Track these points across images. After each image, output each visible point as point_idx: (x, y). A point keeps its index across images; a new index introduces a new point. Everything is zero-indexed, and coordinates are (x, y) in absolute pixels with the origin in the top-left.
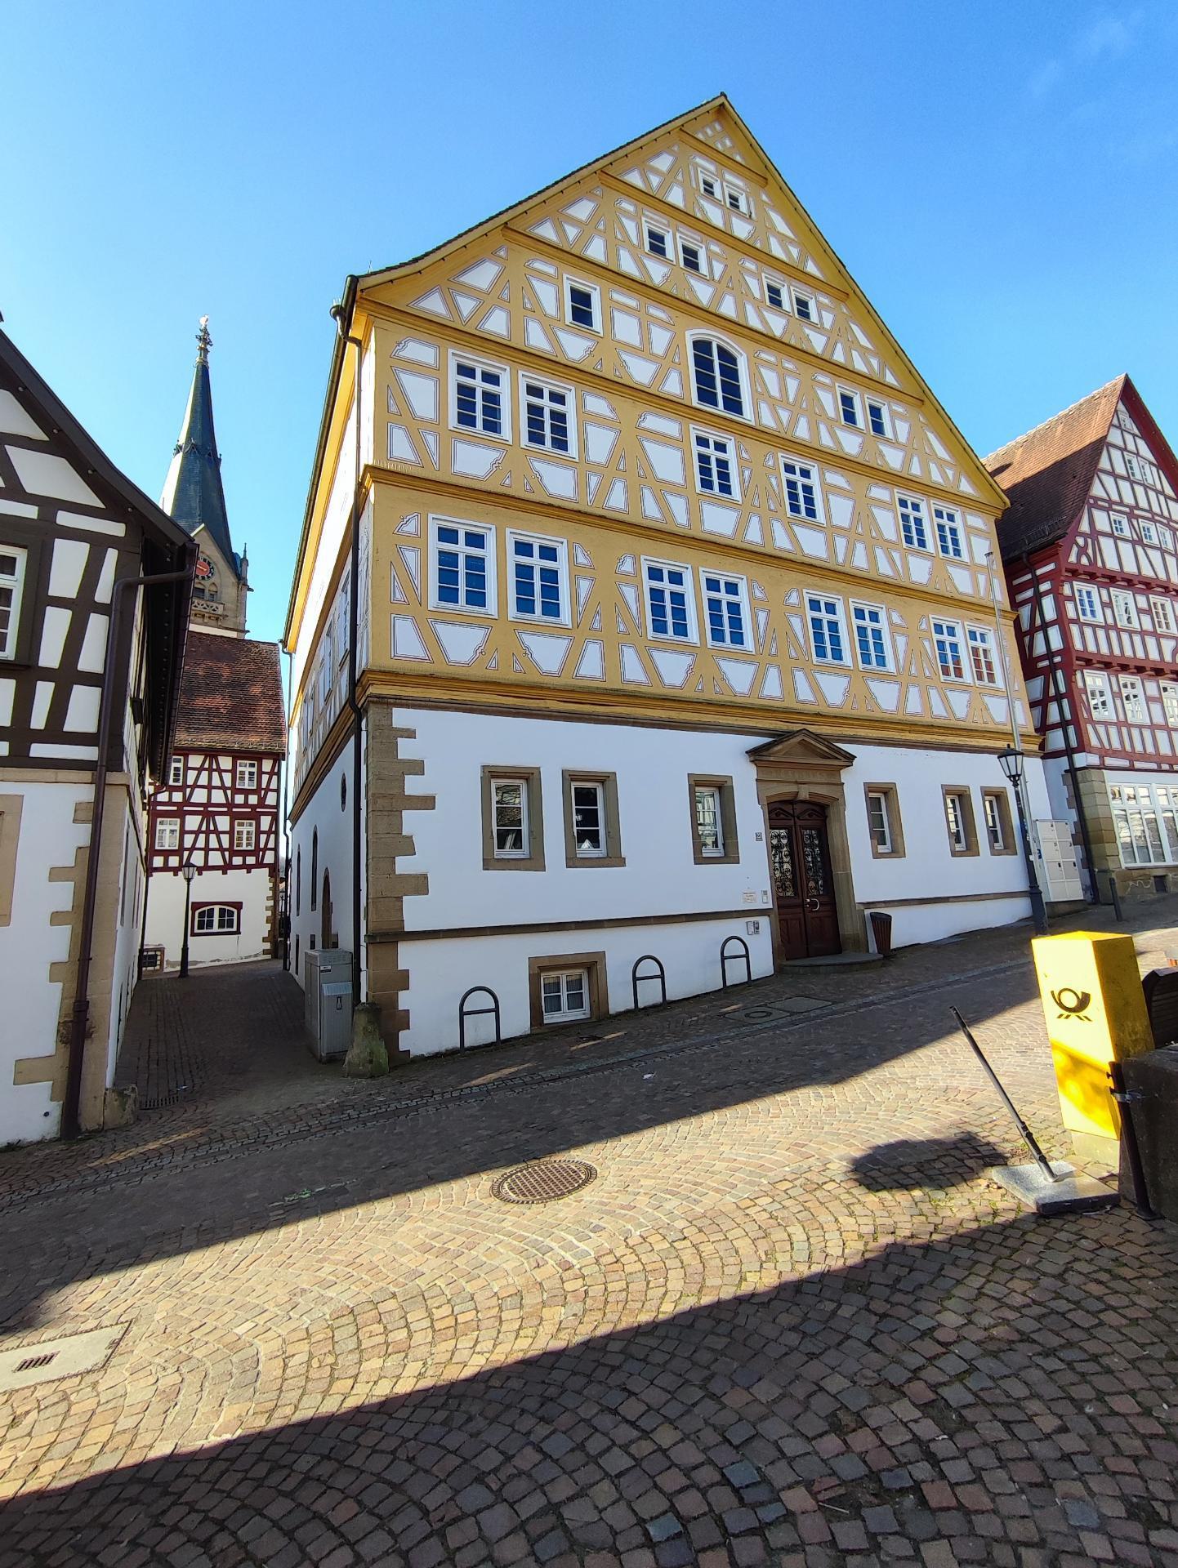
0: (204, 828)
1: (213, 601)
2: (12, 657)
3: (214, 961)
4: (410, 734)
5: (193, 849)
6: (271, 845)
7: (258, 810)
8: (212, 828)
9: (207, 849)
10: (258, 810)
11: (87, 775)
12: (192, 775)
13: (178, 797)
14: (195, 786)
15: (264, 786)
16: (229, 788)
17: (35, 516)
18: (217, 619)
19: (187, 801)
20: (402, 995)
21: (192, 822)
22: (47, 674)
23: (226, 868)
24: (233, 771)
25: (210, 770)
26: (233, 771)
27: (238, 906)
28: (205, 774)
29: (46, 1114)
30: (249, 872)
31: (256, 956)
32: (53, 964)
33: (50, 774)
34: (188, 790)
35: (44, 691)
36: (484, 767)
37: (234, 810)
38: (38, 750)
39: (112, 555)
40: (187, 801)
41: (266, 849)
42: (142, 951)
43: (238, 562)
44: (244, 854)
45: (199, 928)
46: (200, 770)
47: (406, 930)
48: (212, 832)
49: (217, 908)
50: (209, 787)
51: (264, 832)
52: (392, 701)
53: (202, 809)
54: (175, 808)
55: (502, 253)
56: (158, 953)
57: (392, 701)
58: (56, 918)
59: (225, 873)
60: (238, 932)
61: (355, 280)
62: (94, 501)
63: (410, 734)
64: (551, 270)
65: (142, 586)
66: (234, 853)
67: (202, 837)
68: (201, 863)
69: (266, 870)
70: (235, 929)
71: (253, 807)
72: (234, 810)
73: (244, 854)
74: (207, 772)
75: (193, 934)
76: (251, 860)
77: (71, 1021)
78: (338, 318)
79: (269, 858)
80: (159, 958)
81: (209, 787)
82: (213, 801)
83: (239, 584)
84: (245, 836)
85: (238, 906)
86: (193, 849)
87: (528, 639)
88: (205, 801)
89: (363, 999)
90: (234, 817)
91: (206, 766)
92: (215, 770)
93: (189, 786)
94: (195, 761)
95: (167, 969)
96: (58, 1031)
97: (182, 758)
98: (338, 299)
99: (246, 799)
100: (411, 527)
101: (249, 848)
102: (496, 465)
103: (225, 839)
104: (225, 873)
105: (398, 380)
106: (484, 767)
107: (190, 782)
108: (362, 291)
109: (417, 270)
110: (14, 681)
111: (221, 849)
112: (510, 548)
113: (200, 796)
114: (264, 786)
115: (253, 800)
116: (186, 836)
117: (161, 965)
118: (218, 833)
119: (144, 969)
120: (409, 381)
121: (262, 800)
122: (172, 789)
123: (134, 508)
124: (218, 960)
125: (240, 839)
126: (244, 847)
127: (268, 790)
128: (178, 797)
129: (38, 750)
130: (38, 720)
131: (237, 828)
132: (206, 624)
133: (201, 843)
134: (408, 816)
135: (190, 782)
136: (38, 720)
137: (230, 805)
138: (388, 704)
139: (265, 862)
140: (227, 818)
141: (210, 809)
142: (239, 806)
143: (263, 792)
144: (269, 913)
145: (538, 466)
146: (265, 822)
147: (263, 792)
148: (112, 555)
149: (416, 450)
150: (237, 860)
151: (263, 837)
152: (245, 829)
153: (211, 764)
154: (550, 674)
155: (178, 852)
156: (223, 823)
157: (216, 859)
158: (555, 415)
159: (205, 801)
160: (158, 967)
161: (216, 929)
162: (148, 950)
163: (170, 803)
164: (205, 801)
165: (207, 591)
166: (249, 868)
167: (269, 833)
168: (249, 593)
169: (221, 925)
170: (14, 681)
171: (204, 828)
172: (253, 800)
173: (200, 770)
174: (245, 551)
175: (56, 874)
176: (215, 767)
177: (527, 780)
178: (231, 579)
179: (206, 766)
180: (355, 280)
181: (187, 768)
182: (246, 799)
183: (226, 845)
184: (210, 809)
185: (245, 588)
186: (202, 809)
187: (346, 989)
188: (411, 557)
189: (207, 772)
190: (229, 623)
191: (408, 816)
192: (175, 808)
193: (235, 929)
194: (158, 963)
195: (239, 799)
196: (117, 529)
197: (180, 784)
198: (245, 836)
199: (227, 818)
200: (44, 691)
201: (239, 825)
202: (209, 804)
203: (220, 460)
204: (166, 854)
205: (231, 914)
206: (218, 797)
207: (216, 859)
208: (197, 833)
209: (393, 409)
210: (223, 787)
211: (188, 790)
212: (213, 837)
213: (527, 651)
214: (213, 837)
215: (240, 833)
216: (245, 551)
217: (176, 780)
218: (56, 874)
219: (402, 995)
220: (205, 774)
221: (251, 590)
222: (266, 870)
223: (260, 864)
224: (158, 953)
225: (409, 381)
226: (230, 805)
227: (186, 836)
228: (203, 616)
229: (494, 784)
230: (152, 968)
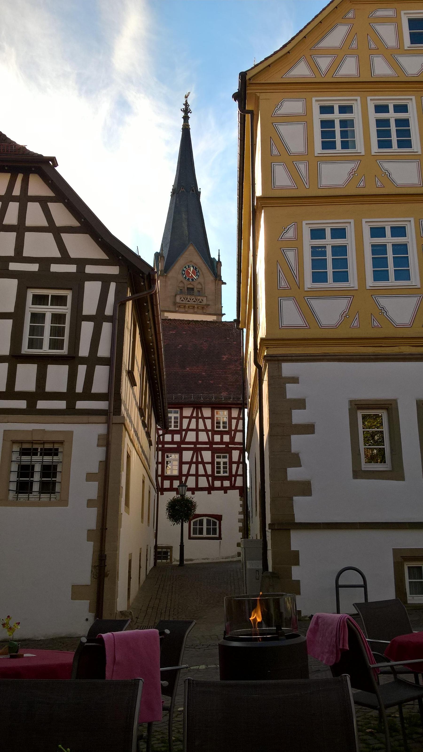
0: (194, 460)
1: (199, 295)
2: (66, 353)
3: (204, 559)
4: (295, 380)
5: (188, 475)
6: (240, 472)
7: (230, 446)
8: (200, 460)
9: (197, 475)
10: (230, 446)
11: (103, 418)
12: (185, 422)
13: (177, 438)
14: (188, 430)
15: (233, 428)
16: (209, 430)
17: (75, 271)
18: (203, 308)
19: (183, 441)
20: (294, 569)
21: (187, 456)
22: (83, 360)
23: (210, 489)
24: (212, 418)
25: (197, 418)
26: (212, 418)
27: (219, 518)
28: (194, 421)
29: (87, 620)
30: (225, 492)
31: (233, 557)
32: (88, 530)
33: (85, 418)
34: (184, 433)
35: (82, 369)
36: (351, 402)
37: (214, 446)
38: (80, 405)
39: (113, 286)
40: (183, 441)
41: (236, 475)
42: (156, 547)
43: (215, 265)
44: (222, 479)
45: (193, 534)
46: (190, 418)
47: (296, 521)
48: (200, 463)
49: (205, 519)
50: (197, 430)
51: (235, 463)
52: (281, 358)
53: (193, 446)
54: (176, 446)
55: (350, 15)
56: (169, 550)
57: (281, 358)
58: (90, 503)
59: (209, 493)
60: (220, 538)
61: (243, 75)
62: (103, 256)
63: (295, 380)
64: (390, 13)
65: (131, 302)
66: (215, 478)
67: (194, 466)
68: (193, 486)
69: (237, 491)
70: (217, 536)
71: (227, 444)
72: (214, 446)
73: (222, 479)
74: (195, 420)
75: (190, 538)
76: (227, 484)
77: (98, 566)
78: (237, 101)
79: (239, 482)
80: (169, 554)
81: (197, 430)
82: (200, 440)
83: (216, 280)
84: (222, 466)
85: (219, 518)
86: (188, 475)
87: (383, 302)
88: (194, 440)
89: (270, 570)
90: (214, 451)
91: (195, 415)
92: (200, 418)
93: (184, 430)
94: (187, 412)
95: (174, 563)
96: (92, 571)
97: (179, 410)
98: (235, 88)
99: (222, 438)
100: (290, 234)
101: (225, 475)
102: (353, 173)
103: (209, 467)
104: (209, 493)
105: (277, 131)
106: (351, 402)
107: (185, 427)
108: (250, 79)
109: (287, 51)
110: (68, 366)
111: (206, 475)
112: (367, 232)
113: (191, 437)
114: (233, 428)
115: (226, 438)
116: (184, 466)
117: (171, 559)
118: (204, 463)
119: (158, 561)
120: (283, 129)
121: (232, 439)
122: (173, 433)
123: (123, 256)
124: (208, 559)
125: (219, 468)
126: (222, 474)
127: (236, 431)
128: (177, 438)
129: (80, 405)
130: (79, 388)
131: (217, 460)
132: (186, 312)
133: (193, 471)
134: (294, 438)
135: (185, 427)
136: (79, 388)
137: (211, 442)
138: (278, 360)
139: (236, 485)
140: (210, 453)
141: (198, 446)
142: (217, 443)
143: (233, 432)
144: (241, 524)
145: (387, 166)
146: (236, 454)
147: (233, 432)
148: (113, 286)
149: (292, 177)
150: (217, 484)
151: (234, 466)
152: (222, 460)
153: (197, 414)
154: (403, 326)
155: (179, 477)
156: (207, 456)
157: (203, 482)
158: (399, 122)
159: (195, 441)
160: (169, 561)
161: (205, 535)
162: (160, 548)
163: (172, 442)
164: (195, 441)
165: (195, 289)
166: (225, 490)
167: (238, 463)
168: (223, 286)
169: (208, 532)
170: (68, 366)
171: (194, 460)
172: (226, 438)
173: (190, 418)
174: (219, 256)
175: (90, 477)
176: (200, 415)
177: (387, 409)
178: (210, 278)
179: (195, 415)
180: (243, 75)
181: (182, 417)
182: (222, 438)
183: (209, 472)
184: (198, 446)
185: (220, 282)
186: (193, 446)
187: (259, 565)
188: (291, 255)
189: (195, 420)
190: (210, 310)
191: (294, 438)
192: (176, 446)
193: (217, 536)
194: (169, 557)
195: (217, 438)
196: (114, 270)
197: (178, 429)
198: (222, 466)
199: (210, 453)
200: (82, 369)
201: (218, 457)
202: (197, 442)
203: (200, 192)
204: (171, 478)
205: (214, 523)
206: (203, 437)
207: (203, 482)
208: (190, 463)
209: (275, 152)
210: (206, 430)
211: (184, 433)
212: (201, 466)
213: (383, 311)
214: (201, 466)
215: (218, 463)
216: (219, 256)
217: (176, 426)
218: (90, 477)
219: (294, 569)
220: (194, 421)
221: (225, 283)
222: (237, 491)
223: (233, 487)
224: (169, 550)
225: (283, 129)
226: (211, 442)
227: (184, 466)
228: (194, 307)
229: (360, 414)
230: (165, 561)
